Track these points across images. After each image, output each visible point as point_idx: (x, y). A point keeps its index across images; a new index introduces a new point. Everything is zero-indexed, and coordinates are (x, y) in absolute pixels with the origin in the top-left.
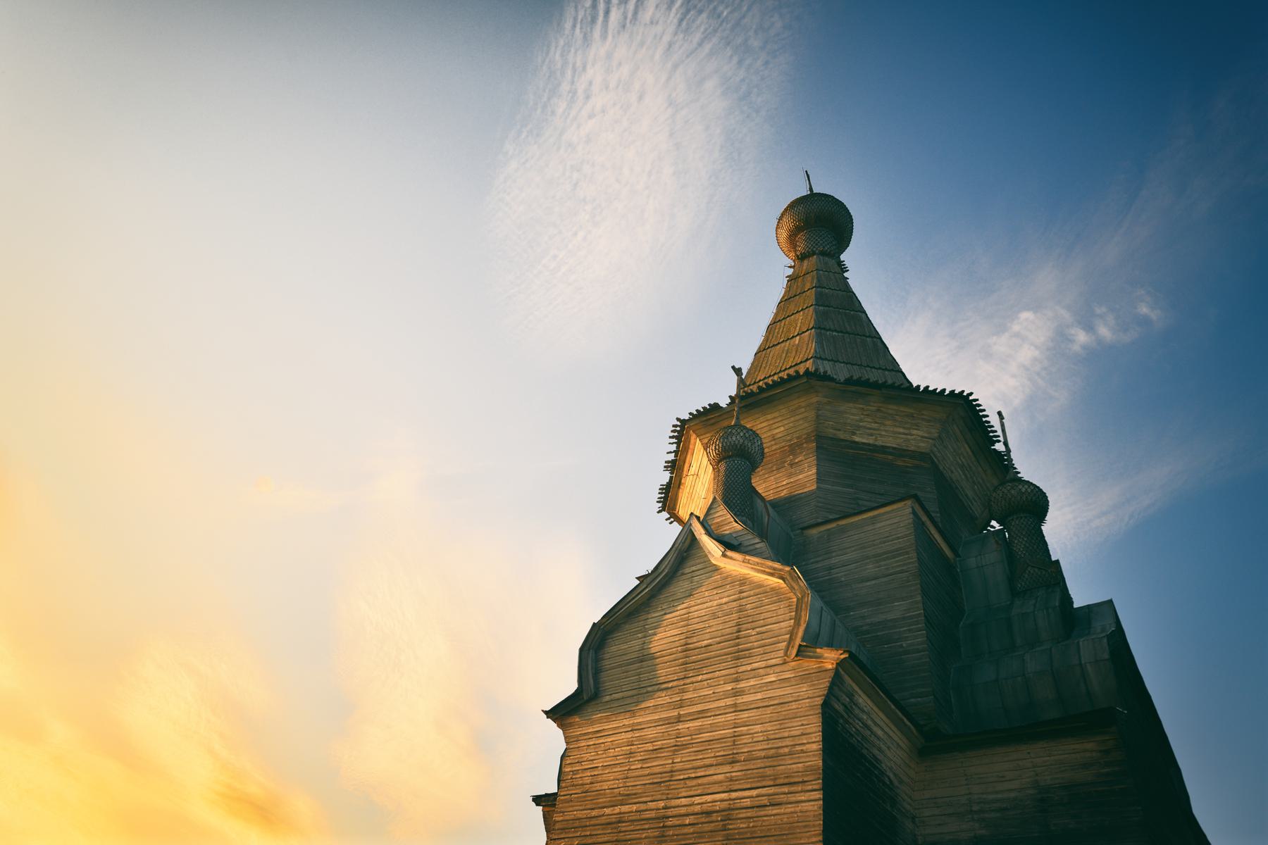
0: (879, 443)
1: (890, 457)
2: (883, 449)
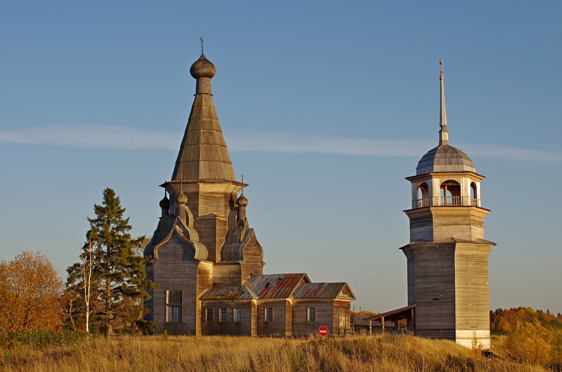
0: (213, 191)
1: (215, 195)
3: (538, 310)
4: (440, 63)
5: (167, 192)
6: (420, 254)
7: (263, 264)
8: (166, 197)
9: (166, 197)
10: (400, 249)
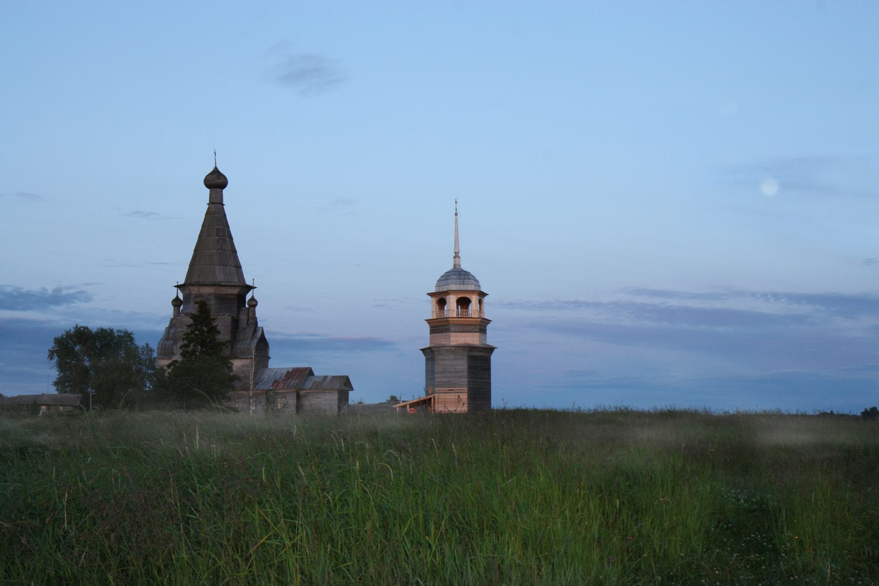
2: (228, 294)
3: (459, 253)
4: (253, 280)
5: (178, 289)
6: (440, 354)
7: (269, 358)
8: (177, 297)
9: (177, 297)
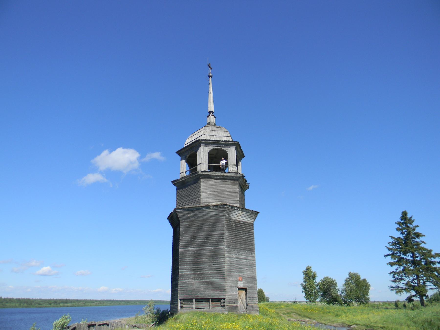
10: (390, 237)
